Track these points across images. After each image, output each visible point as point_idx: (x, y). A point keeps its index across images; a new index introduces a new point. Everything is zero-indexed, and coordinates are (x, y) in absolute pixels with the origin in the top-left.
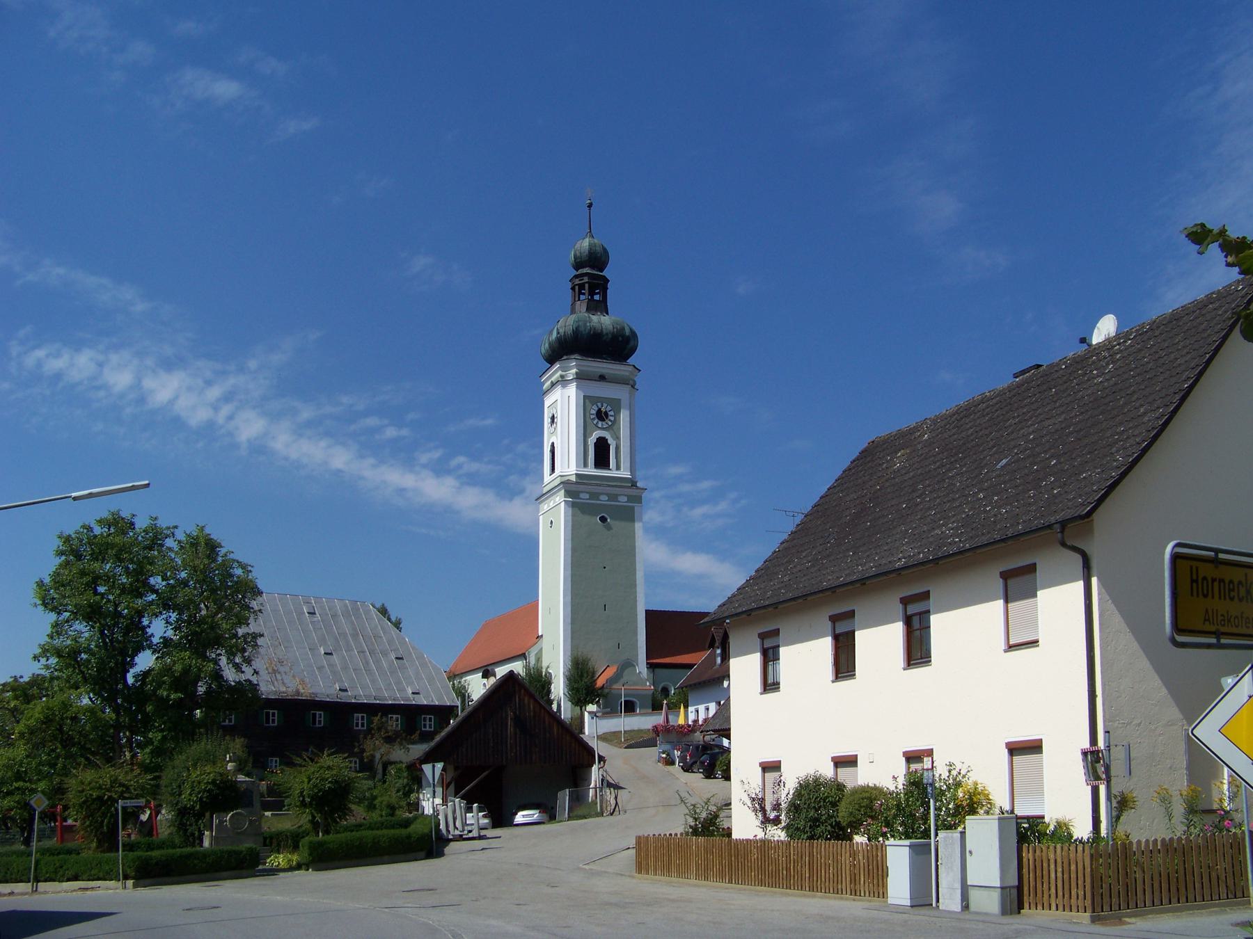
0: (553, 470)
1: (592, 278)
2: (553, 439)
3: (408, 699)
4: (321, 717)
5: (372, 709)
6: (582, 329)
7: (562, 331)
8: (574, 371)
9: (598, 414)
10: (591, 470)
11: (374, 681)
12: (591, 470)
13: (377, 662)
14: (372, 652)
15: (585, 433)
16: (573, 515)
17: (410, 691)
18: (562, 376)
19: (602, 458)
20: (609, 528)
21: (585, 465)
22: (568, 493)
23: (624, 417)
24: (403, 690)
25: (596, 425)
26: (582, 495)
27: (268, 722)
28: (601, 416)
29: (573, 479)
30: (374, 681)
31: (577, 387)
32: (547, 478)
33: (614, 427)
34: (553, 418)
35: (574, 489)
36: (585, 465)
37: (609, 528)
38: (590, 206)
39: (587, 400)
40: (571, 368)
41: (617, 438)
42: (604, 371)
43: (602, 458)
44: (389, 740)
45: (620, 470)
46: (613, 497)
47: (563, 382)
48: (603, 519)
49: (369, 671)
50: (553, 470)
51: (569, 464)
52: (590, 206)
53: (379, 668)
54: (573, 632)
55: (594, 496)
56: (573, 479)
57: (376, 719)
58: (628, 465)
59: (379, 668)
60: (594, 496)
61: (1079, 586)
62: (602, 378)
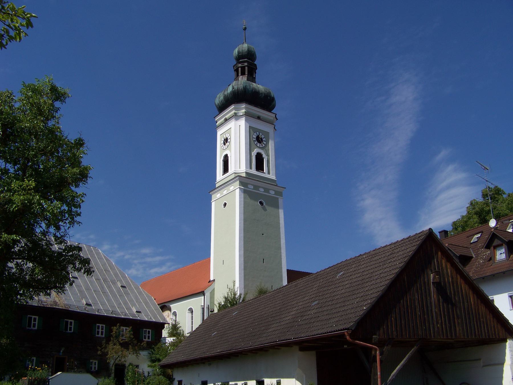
0: (226, 169)
1: (247, 63)
2: (227, 152)
3: (133, 315)
4: (72, 325)
5: (111, 322)
6: (248, 87)
7: (236, 87)
8: (244, 111)
9: (257, 139)
10: (254, 171)
11: (109, 300)
12: (254, 171)
13: (109, 287)
14: (105, 280)
15: (250, 149)
16: (245, 198)
17: (134, 310)
18: (235, 113)
19: (260, 166)
20: (265, 210)
21: (251, 168)
22: (242, 183)
23: (271, 145)
24: (129, 309)
25: (256, 145)
26: (250, 186)
27: (30, 326)
28: (259, 140)
29: (244, 175)
30: (109, 300)
31: (246, 120)
32: (220, 175)
33: (265, 148)
34: (226, 141)
35: (246, 182)
36: (251, 168)
37: (265, 210)
38: (245, 29)
39: (251, 130)
40: (242, 109)
41: (268, 155)
42: (260, 114)
43: (260, 166)
44: (125, 345)
45: (270, 173)
46: (267, 190)
47: (236, 116)
48: (261, 203)
49: (104, 293)
50: (226, 169)
51: (240, 164)
52: (245, 29)
53: (112, 291)
54: (245, 276)
55: (256, 187)
56: (244, 175)
57: (115, 329)
58: (274, 172)
59: (112, 291)
60: (256, 187)
61: (203, 297)
62: (259, 118)
